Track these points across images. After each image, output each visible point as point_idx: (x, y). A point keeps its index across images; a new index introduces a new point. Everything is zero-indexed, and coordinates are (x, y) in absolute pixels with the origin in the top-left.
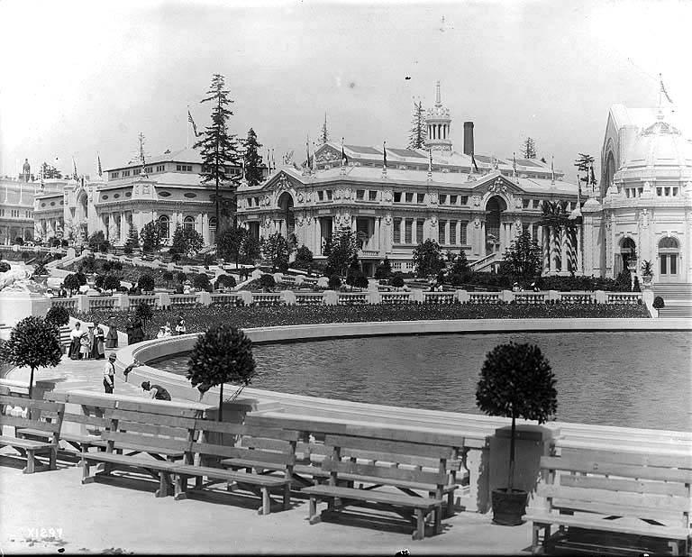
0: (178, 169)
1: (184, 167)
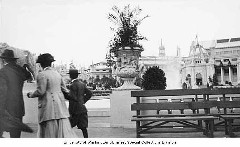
0: (103, 64)
1: (104, 64)
